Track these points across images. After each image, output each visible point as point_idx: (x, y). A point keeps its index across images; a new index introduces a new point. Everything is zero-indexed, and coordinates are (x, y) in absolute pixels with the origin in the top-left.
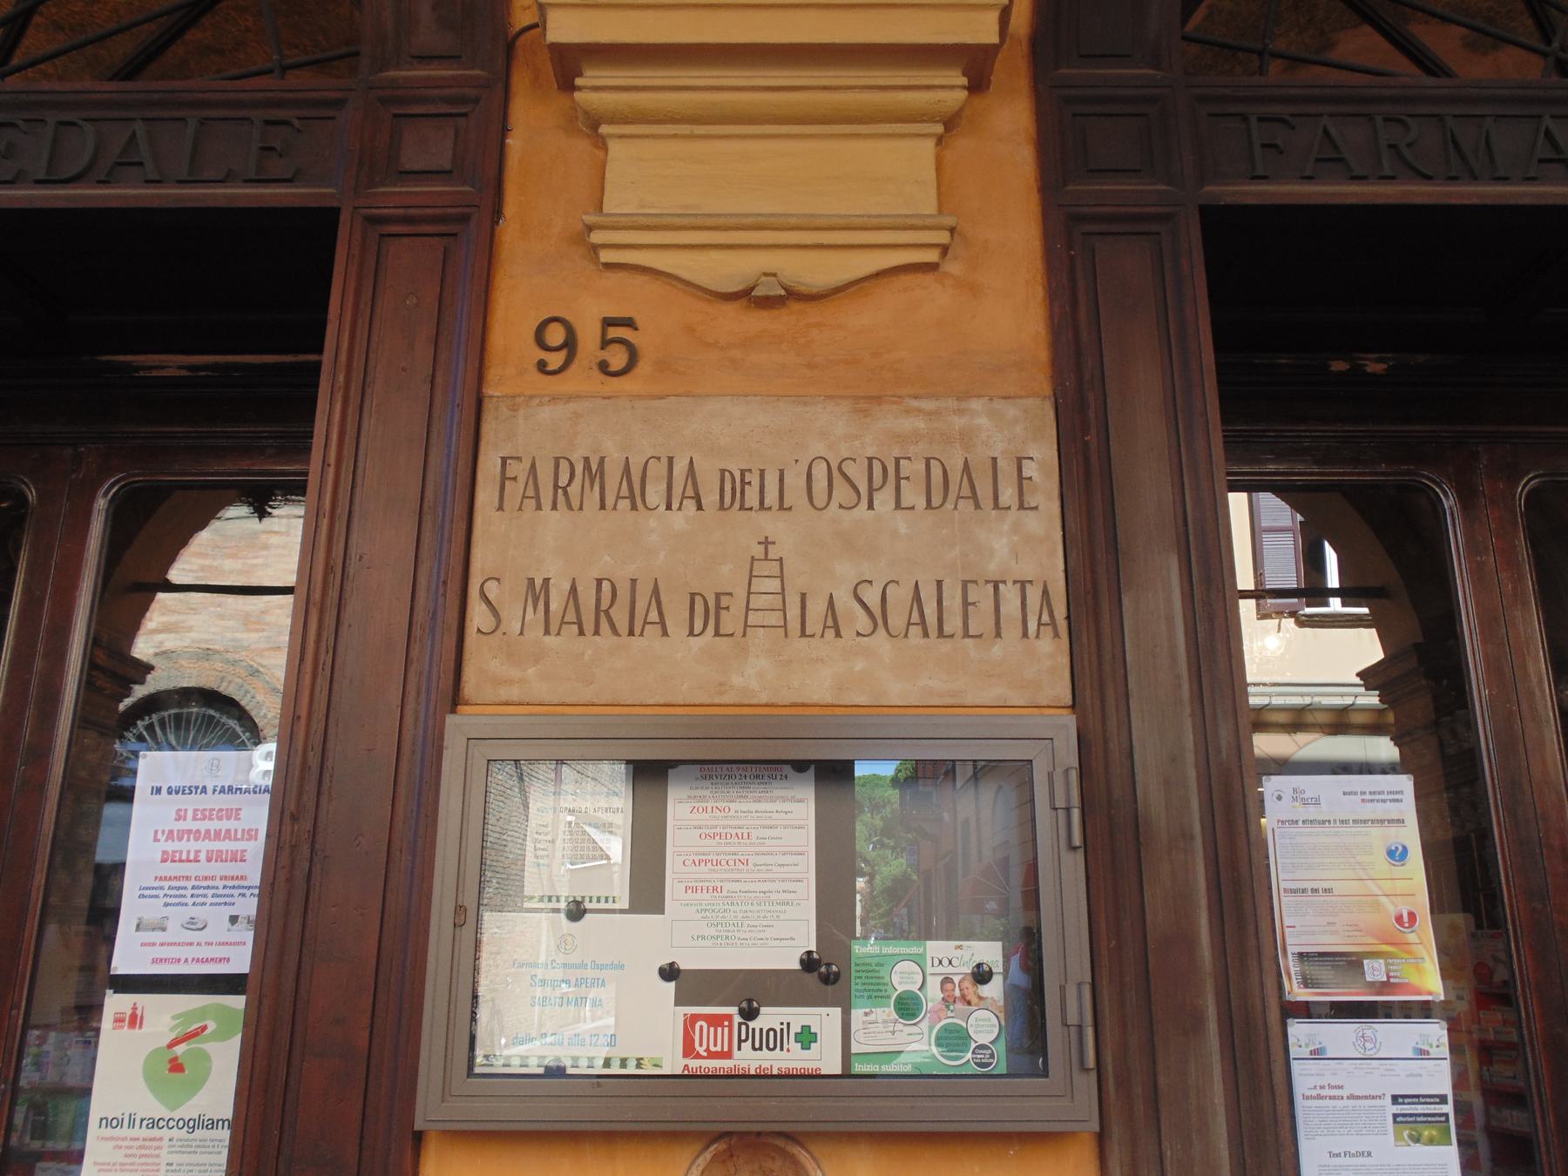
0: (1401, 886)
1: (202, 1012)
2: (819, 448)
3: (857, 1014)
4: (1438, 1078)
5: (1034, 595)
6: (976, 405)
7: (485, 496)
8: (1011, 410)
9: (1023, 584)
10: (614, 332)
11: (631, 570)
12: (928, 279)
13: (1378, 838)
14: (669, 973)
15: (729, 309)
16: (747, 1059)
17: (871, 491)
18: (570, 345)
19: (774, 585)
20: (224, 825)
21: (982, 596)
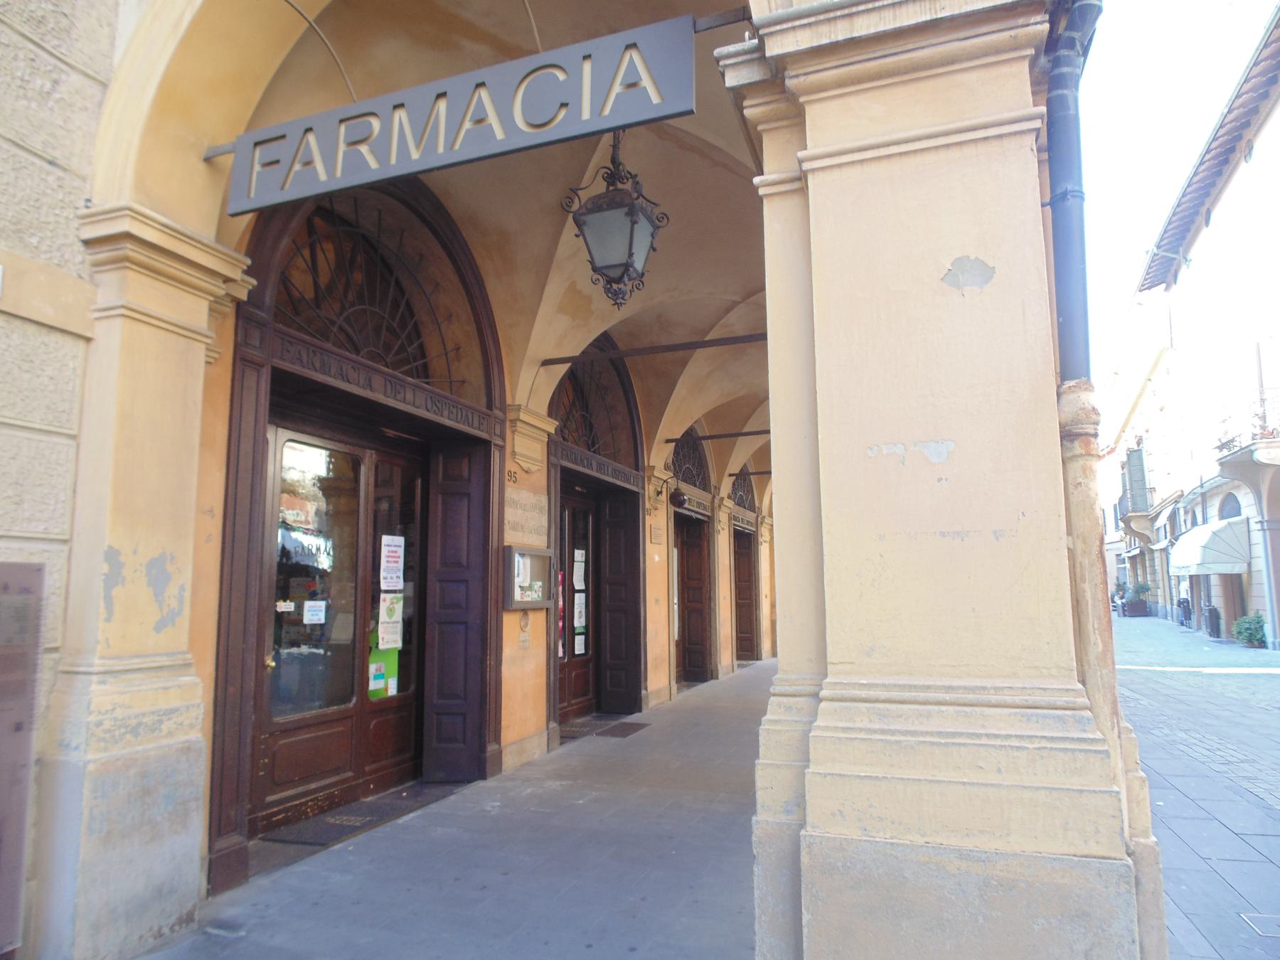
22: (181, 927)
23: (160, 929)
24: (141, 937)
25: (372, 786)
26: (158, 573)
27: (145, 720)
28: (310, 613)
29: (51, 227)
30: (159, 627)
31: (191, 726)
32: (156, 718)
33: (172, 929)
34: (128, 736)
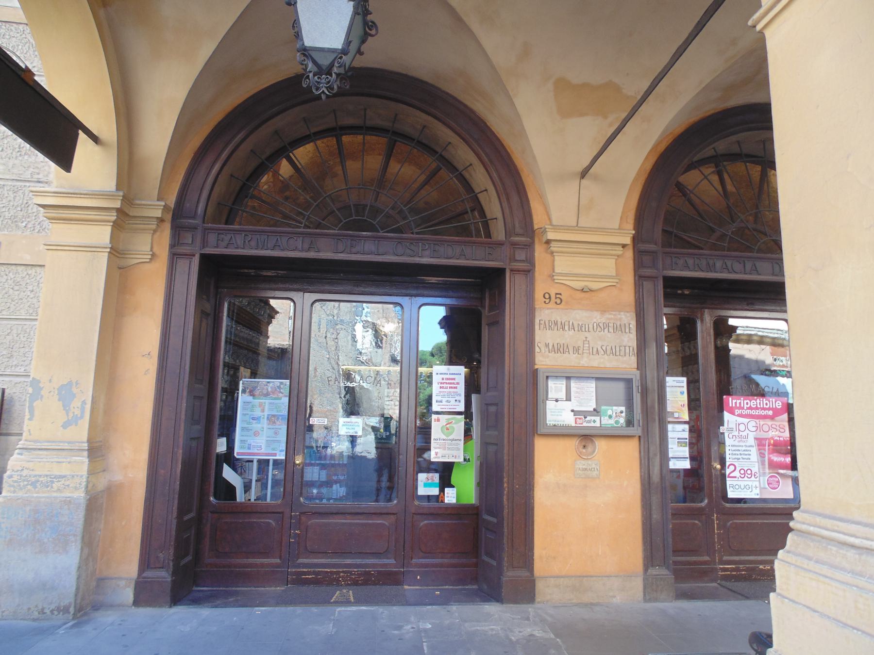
0: (682, 399)
1: (452, 419)
2: (595, 320)
3: (602, 418)
4: (686, 435)
5: (631, 349)
6: (622, 313)
7: (537, 327)
8: (628, 315)
9: (629, 347)
10: (558, 296)
11: (563, 342)
12: (613, 287)
13: (679, 390)
14: (572, 411)
15: (578, 292)
16: (585, 424)
17: (604, 329)
18: (550, 298)
19: (588, 345)
20: (452, 381)
21: (623, 349)
22: (59, 613)
23: (43, 609)
24: (29, 609)
25: (419, 577)
26: (66, 393)
27: (41, 479)
28: (345, 427)
29: (35, 214)
30: (65, 426)
31: (76, 489)
32: (49, 479)
33: (52, 612)
34: (29, 487)
